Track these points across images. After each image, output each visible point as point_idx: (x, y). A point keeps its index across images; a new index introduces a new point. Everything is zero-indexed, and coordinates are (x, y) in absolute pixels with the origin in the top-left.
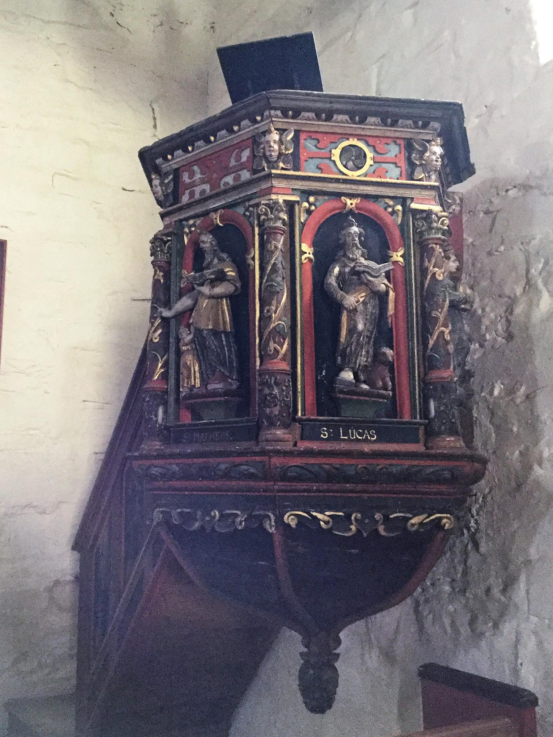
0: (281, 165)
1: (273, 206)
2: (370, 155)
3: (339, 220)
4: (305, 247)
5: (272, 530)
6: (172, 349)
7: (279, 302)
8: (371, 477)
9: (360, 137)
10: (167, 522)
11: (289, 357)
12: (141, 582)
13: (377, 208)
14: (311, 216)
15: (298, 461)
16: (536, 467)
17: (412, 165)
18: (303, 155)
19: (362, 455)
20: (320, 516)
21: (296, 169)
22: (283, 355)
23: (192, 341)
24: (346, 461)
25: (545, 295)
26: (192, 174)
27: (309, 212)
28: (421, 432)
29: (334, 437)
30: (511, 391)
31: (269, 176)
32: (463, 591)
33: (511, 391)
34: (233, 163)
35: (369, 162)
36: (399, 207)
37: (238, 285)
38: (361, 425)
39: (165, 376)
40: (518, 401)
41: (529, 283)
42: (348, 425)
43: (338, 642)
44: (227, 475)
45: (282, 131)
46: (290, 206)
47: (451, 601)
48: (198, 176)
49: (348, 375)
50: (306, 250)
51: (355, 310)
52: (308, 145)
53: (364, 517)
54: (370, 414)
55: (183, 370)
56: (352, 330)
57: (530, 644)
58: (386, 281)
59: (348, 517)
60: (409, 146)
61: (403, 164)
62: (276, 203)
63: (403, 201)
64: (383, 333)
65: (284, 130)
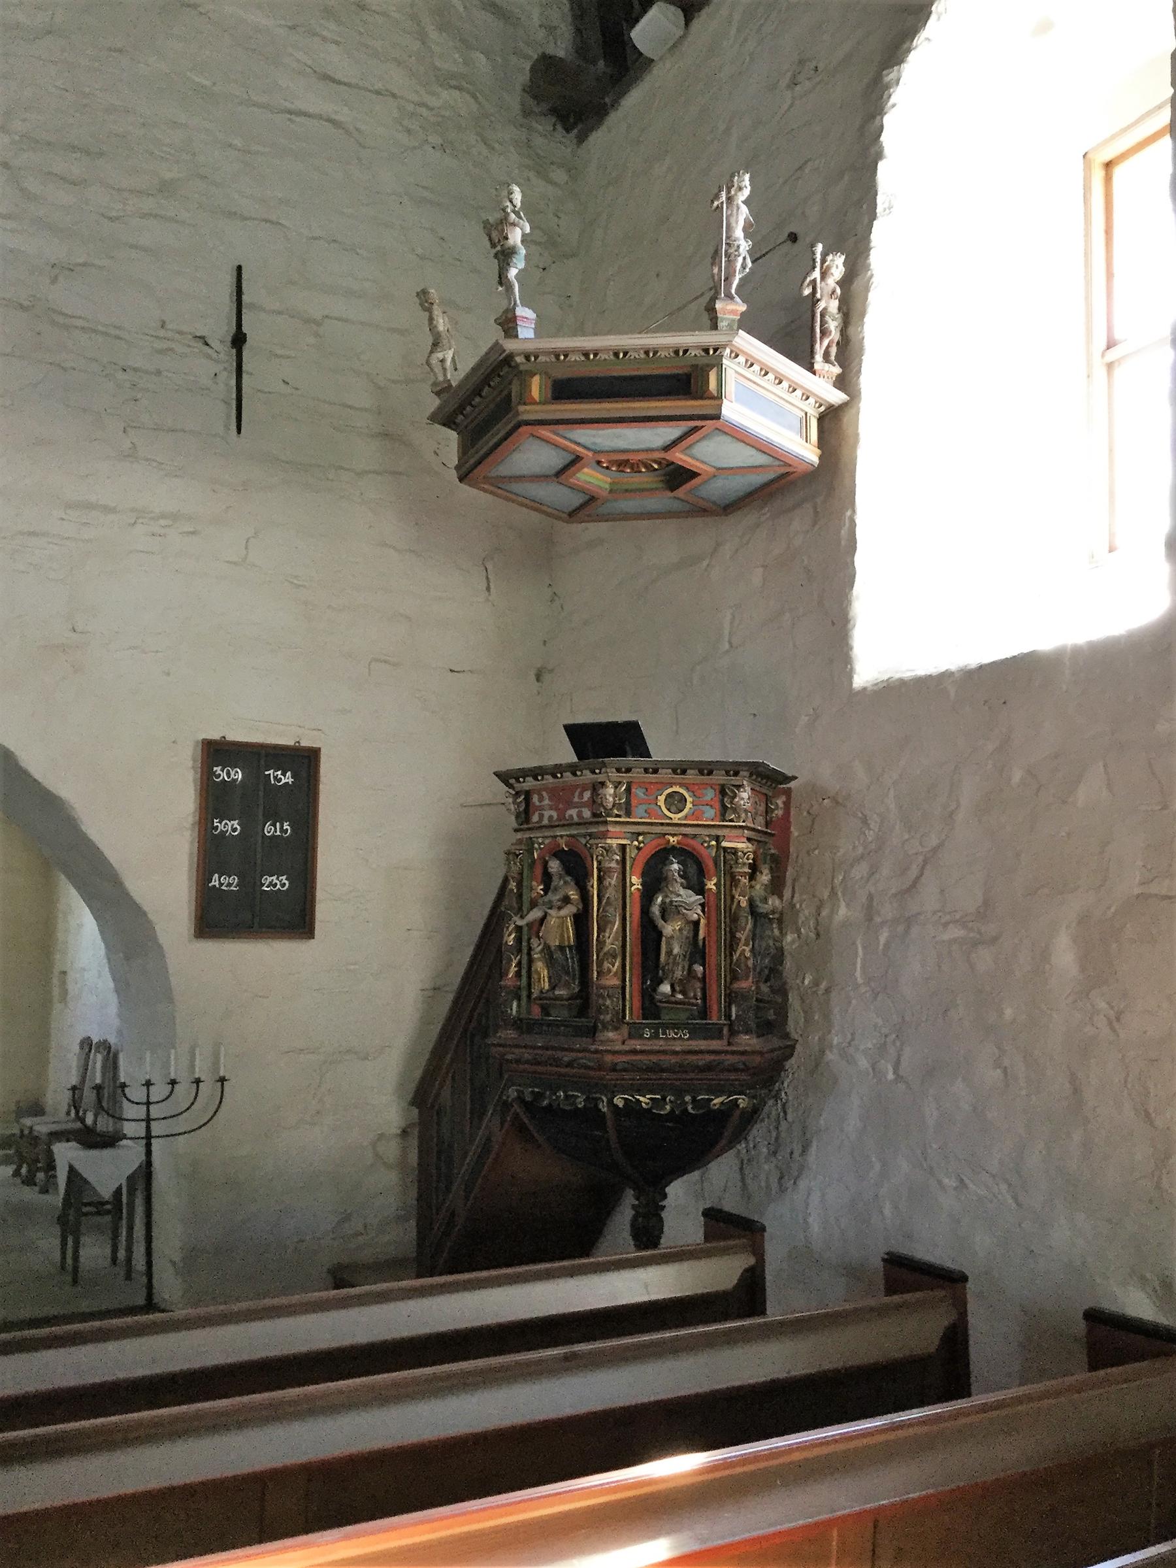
0: (616, 812)
1: (608, 850)
2: (689, 799)
3: (662, 855)
4: (635, 879)
5: (605, 1110)
6: (525, 951)
7: (612, 929)
8: (683, 1068)
9: (681, 785)
10: (520, 1099)
11: (620, 972)
12: (489, 1139)
13: (695, 844)
14: (640, 852)
15: (625, 1058)
16: (827, 1052)
17: (724, 808)
18: (634, 802)
19: (676, 1053)
20: (641, 1099)
21: (628, 814)
22: (613, 973)
23: (542, 950)
24: (662, 1058)
25: (843, 904)
26: (541, 799)
27: (639, 849)
28: (725, 1031)
29: (655, 1036)
30: (816, 983)
31: (606, 822)
32: (775, 1153)
33: (816, 983)
34: (576, 799)
35: (689, 805)
36: (714, 843)
37: (580, 907)
38: (675, 1026)
39: (518, 974)
40: (820, 993)
41: (833, 893)
42: (666, 1027)
43: (665, 1196)
44: (569, 1065)
45: (617, 785)
46: (623, 848)
47: (767, 1160)
48: (546, 802)
49: (666, 988)
50: (636, 882)
51: (672, 937)
52: (638, 792)
53: (677, 1099)
54: (683, 1016)
55: (535, 976)
56: (669, 953)
57: (815, 1198)
58: (699, 912)
59: (664, 1098)
60: (723, 792)
61: (718, 805)
62: (610, 846)
63: (717, 839)
64: (697, 952)
65: (620, 783)
